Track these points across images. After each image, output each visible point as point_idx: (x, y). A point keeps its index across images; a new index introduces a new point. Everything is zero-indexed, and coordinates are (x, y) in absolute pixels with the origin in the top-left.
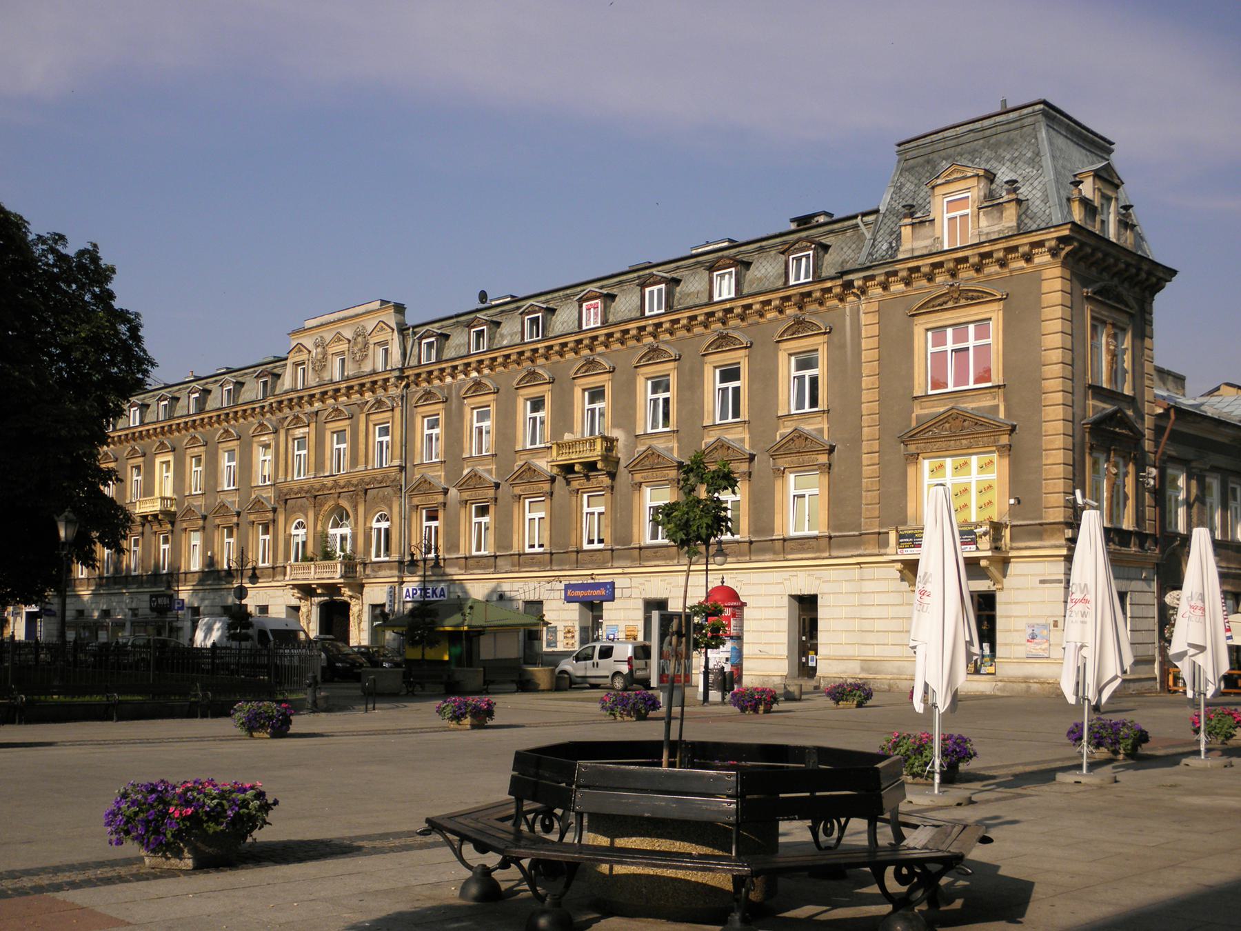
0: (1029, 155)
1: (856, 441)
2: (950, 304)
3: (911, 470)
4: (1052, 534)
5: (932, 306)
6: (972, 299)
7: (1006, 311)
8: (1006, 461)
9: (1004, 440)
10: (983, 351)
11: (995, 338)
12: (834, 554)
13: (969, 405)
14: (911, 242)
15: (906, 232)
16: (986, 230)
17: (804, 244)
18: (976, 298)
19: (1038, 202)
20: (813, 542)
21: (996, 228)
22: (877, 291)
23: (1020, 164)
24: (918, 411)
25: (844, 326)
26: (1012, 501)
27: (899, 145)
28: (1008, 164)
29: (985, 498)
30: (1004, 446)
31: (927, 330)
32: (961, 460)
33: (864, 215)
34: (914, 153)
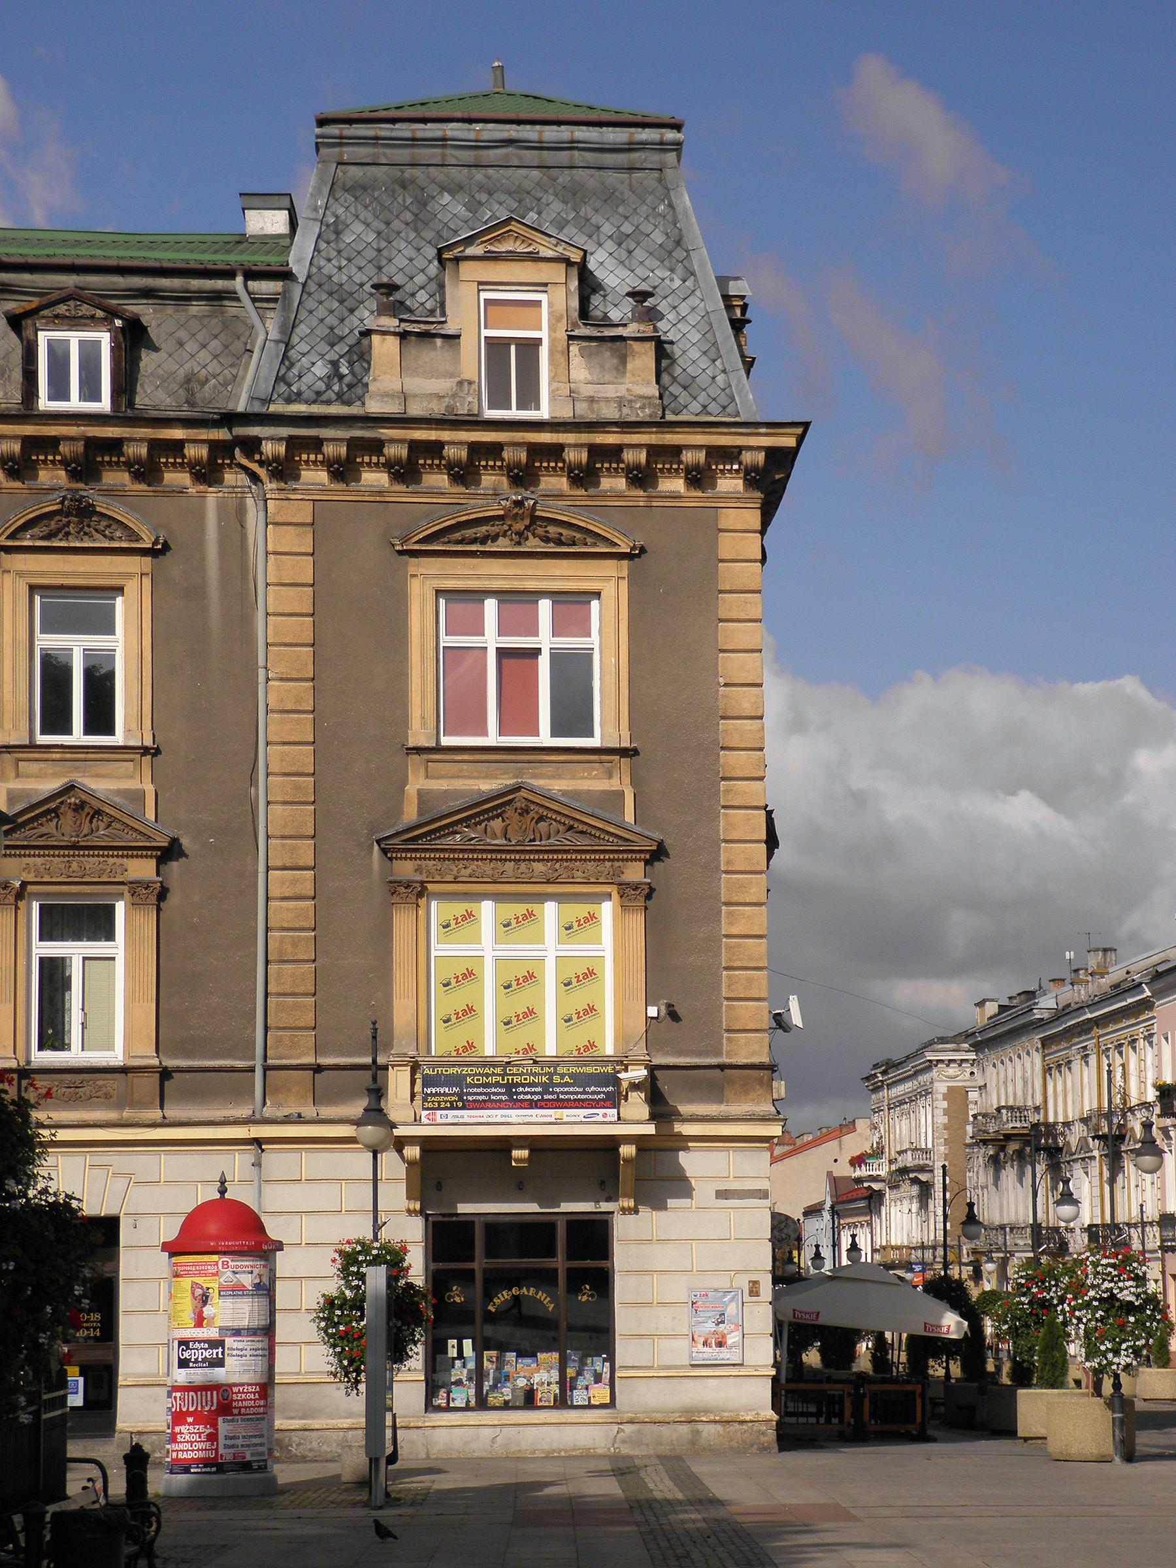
0: (658, 237)
1: (241, 830)
2: (503, 544)
3: (402, 922)
4: (745, 1090)
5: (457, 538)
6: (559, 542)
7: (635, 582)
8: (637, 921)
9: (635, 872)
10: (572, 671)
11: (603, 636)
12: (172, 1112)
13: (556, 784)
14: (398, 381)
15: (385, 349)
16: (587, 390)
17: (86, 309)
18: (571, 543)
19: (694, 354)
20: (113, 1083)
21: (611, 391)
22: (315, 477)
23: (640, 254)
24: (417, 783)
25: (201, 542)
26: (653, 1011)
27: (322, 122)
28: (610, 245)
29: (579, 999)
30: (636, 887)
31: (439, 593)
32: (580, 910)
33: (251, 275)
34: (362, 153)
